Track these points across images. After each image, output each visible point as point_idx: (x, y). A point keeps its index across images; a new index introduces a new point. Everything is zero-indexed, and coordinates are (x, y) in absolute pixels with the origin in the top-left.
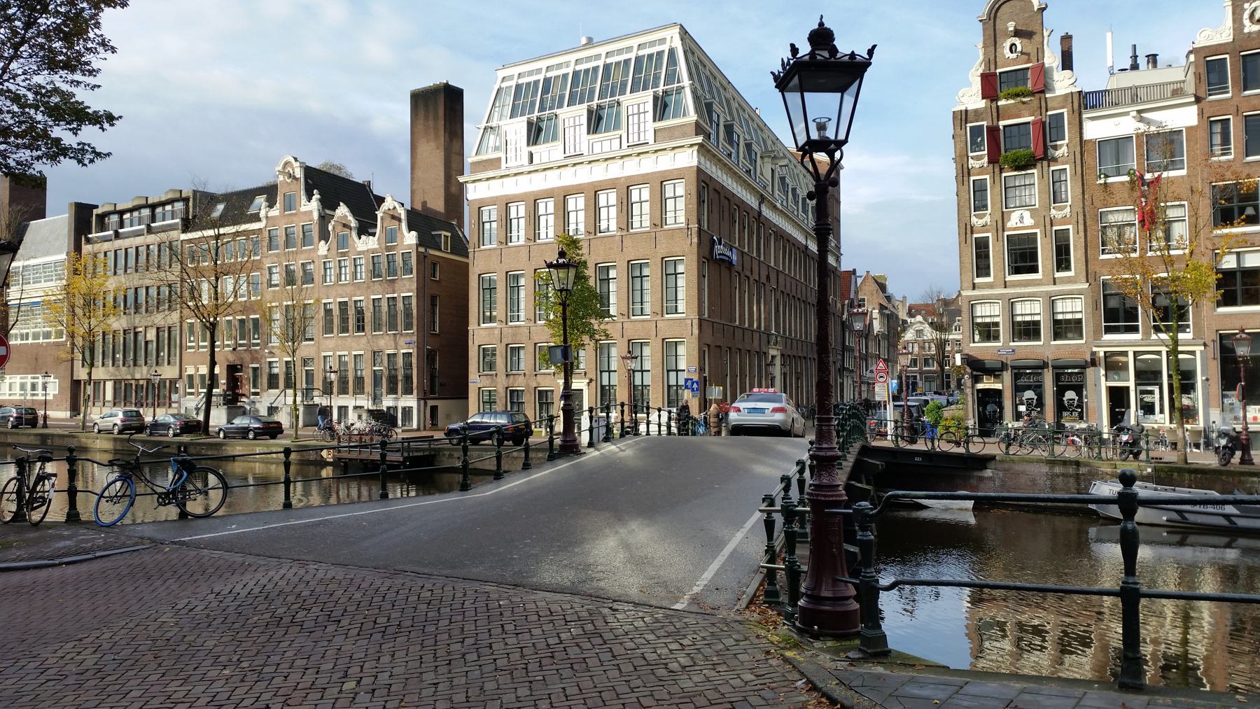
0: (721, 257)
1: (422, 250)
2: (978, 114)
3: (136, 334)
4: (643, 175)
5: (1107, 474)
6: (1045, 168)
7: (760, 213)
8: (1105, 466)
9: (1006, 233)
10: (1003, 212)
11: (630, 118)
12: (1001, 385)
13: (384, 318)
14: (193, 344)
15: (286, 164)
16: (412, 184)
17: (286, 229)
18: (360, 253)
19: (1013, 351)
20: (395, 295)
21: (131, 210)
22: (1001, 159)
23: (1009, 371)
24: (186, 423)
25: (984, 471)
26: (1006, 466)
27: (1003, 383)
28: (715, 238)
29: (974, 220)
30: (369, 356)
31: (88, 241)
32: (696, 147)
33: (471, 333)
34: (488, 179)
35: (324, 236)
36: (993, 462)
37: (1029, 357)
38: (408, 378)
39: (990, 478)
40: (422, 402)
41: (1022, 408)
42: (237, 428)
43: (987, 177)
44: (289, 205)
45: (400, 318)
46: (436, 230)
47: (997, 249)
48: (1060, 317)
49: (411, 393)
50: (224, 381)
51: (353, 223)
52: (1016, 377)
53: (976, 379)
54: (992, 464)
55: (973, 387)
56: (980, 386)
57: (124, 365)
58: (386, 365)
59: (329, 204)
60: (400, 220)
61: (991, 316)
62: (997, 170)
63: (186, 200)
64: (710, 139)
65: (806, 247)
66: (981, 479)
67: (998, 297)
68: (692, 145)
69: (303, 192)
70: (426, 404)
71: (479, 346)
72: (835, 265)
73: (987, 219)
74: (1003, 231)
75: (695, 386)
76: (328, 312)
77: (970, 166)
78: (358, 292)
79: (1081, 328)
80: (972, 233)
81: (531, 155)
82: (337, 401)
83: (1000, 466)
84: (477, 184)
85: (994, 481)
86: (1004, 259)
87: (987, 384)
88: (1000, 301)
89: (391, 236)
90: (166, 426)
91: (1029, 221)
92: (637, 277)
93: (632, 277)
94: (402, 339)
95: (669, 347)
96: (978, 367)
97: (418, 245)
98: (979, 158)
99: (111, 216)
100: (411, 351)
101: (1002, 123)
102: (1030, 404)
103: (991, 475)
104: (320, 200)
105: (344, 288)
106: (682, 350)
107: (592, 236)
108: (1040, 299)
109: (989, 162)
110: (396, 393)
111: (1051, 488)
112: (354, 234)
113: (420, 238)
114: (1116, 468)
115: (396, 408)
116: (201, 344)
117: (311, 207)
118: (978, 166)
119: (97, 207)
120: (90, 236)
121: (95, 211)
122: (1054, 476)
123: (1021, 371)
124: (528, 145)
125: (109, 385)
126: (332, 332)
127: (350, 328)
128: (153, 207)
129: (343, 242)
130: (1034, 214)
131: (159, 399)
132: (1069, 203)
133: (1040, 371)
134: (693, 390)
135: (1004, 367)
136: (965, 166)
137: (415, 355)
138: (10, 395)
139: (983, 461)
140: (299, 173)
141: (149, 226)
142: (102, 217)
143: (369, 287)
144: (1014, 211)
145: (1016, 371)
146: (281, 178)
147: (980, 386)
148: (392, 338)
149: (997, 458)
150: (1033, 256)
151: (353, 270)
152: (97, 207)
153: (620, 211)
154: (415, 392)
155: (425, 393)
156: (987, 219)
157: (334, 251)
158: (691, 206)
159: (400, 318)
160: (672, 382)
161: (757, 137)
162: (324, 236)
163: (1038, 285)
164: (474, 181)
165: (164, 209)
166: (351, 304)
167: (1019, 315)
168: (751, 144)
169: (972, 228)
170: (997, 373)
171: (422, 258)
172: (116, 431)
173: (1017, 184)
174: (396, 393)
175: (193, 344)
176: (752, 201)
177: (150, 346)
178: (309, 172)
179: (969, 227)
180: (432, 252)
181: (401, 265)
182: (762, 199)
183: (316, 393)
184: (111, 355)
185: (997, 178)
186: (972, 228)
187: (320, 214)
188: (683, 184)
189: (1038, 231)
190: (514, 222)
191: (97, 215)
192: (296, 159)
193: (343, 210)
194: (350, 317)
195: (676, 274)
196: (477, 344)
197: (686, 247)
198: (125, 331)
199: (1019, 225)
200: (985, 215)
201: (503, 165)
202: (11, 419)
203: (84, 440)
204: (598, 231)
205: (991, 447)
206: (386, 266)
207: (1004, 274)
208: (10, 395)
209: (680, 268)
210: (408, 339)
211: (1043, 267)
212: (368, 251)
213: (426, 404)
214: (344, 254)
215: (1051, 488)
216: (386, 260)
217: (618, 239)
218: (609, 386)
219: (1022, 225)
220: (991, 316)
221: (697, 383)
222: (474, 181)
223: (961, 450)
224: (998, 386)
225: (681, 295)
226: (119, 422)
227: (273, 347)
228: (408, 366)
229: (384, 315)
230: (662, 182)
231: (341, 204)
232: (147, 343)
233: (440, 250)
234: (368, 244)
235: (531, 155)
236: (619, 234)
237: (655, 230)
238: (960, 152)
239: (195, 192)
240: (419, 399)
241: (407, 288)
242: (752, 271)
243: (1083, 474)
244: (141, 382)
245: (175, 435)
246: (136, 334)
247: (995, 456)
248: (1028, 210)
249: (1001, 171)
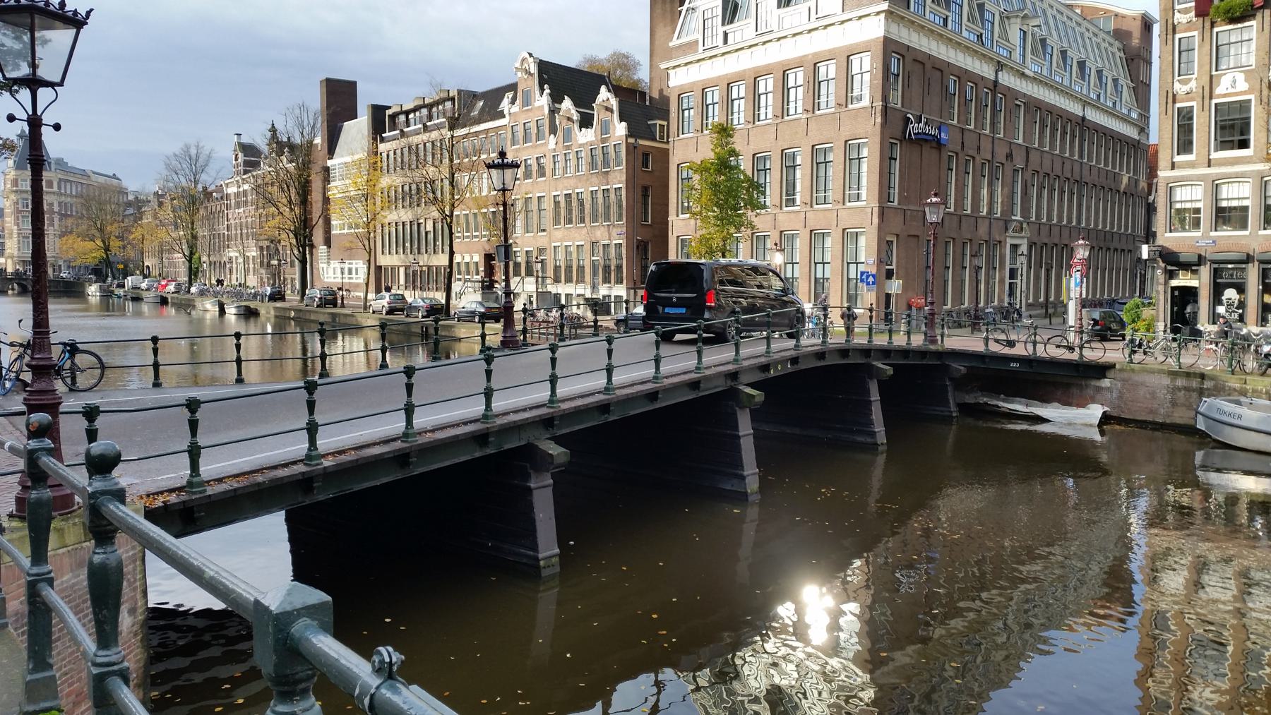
1: (631, 140)
3: (419, 225)
4: (830, 51)
5: (1235, 390)
7: (996, 83)
8: (1233, 381)
9: (1214, 101)
10: (1211, 77)
11: (706, 22)
12: (1197, 282)
13: (600, 210)
14: (460, 235)
15: (524, 60)
16: (651, 72)
17: (524, 124)
18: (581, 145)
19: (1214, 242)
20: (609, 187)
21: (414, 110)
22: (1212, 11)
23: (1208, 266)
24: (432, 307)
25: (1102, 380)
26: (1126, 375)
27: (1200, 280)
29: (1177, 86)
30: (588, 247)
31: (383, 140)
32: (883, 15)
33: (670, 224)
34: (686, 64)
35: (553, 130)
36: (1113, 370)
37: (1232, 249)
38: (619, 267)
39: (1108, 389)
40: (632, 291)
41: (1221, 310)
42: (467, 312)
43: (1195, 33)
44: (527, 102)
45: (613, 209)
46: (652, 120)
47: (1202, 120)
48: (1224, 204)
49: (622, 283)
50: (483, 269)
51: (576, 117)
52: (1216, 273)
53: (1171, 275)
54: (1111, 374)
55: (1166, 283)
57: (411, 253)
58: (602, 255)
59: (556, 98)
60: (612, 111)
61: (1192, 201)
62: (1208, 25)
63: (453, 99)
64: (908, 8)
66: (1099, 389)
67: (1200, 178)
68: (878, 13)
69: (537, 87)
70: (635, 293)
71: (678, 237)
73: (1193, 84)
74: (1211, 98)
75: (871, 279)
76: (557, 203)
77: (1176, 22)
78: (580, 185)
79: (1246, 217)
80: (1174, 102)
81: (726, 35)
82: (563, 289)
83: (1119, 375)
84: (677, 69)
85: (1112, 392)
86: (1209, 133)
87: (1184, 280)
88: (1202, 183)
89: (605, 128)
90: (417, 309)
91: (1242, 85)
92: (762, 170)
93: (817, 163)
94: (615, 230)
95: (847, 237)
96: (1173, 261)
97: (627, 137)
98: (1186, 11)
99: (400, 116)
100: (621, 241)
102: (1230, 305)
103: (1109, 385)
104: (550, 95)
105: (569, 180)
106: (862, 241)
107: (779, 120)
108: (1250, 180)
109: (1197, 16)
110: (610, 282)
111: (1171, 402)
112: (576, 127)
113: (629, 128)
114: (1245, 383)
115: (609, 296)
116: (466, 234)
117: (542, 101)
118: (1184, 21)
119: (389, 108)
120: (384, 135)
121: (389, 112)
122: (1176, 389)
123: (1222, 266)
124: (723, 24)
125: (402, 270)
126: (560, 224)
127: (574, 219)
128: (430, 107)
129: (567, 136)
131: (437, 284)
133: (1244, 266)
134: (868, 284)
135: (1201, 260)
136: (1170, 22)
137: (624, 245)
138: (334, 278)
139: (1101, 370)
140: (533, 69)
141: (425, 126)
142: (393, 117)
143: (588, 180)
144: (1225, 74)
145: (1216, 266)
146: (519, 74)
147: (1174, 283)
148: (606, 229)
149: (1117, 366)
150: (1245, 127)
151: (576, 163)
152: (389, 108)
153: (806, 92)
154: (625, 281)
155: (635, 283)
156: (1193, 84)
157: (560, 145)
158: (876, 82)
159: (613, 209)
160: (852, 275)
162: (553, 130)
163: (1249, 163)
164: (674, 67)
165: (438, 108)
166: (574, 196)
167: (1178, 202)
169: (1174, 96)
170: (1194, 268)
171: (631, 149)
172: (384, 312)
173: (1232, 40)
174: (610, 282)
175: (460, 235)
176: (987, 71)
177: (429, 236)
178: (544, 67)
179: (1170, 95)
180: (642, 142)
181: (614, 157)
182: (1000, 66)
183: (548, 281)
184: (402, 244)
185: (1207, 34)
186: (1174, 96)
187: (550, 108)
189: (1251, 97)
190: (857, 79)
191: (389, 116)
192: (531, 55)
193: (567, 104)
194: (574, 208)
195: (859, 159)
196: (675, 235)
197: (869, 128)
198: (411, 222)
200: (1190, 80)
201: (701, 48)
202: (317, 299)
203: (359, 319)
204: (756, 119)
205: (1113, 353)
206: (602, 159)
207: (1209, 151)
208: (334, 278)
209: (865, 152)
210: (619, 230)
211: (1255, 141)
212: (587, 143)
213: (635, 293)
214: (568, 148)
215: (1171, 402)
216: (601, 152)
217: (804, 122)
218: (793, 278)
220: (1192, 201)
221: (874, 276)
222: (674, 67)
223: (1075, 356)
224: (1194, 283)
225: (864, 181)
226: (386, 305)
227: (517, 238)
228: (619, 257)
229: (600, 206)
230: (703, 89)
231: (566, 97)
232: (426, 233)
233: (654, 139)
234: (586, 137)
235: (726, 35)
236: (805, 116)
237: (839, 111)
238: (1165, 5)
239: (459, 92)
240: (628, 289)
241: (618, 180)
242: (979, 148)
243: (1208, 389)
244: (424, 268)
245: (423, 317)
246: (419, 225)
247: (1115, 365)
249: (1213, 25)
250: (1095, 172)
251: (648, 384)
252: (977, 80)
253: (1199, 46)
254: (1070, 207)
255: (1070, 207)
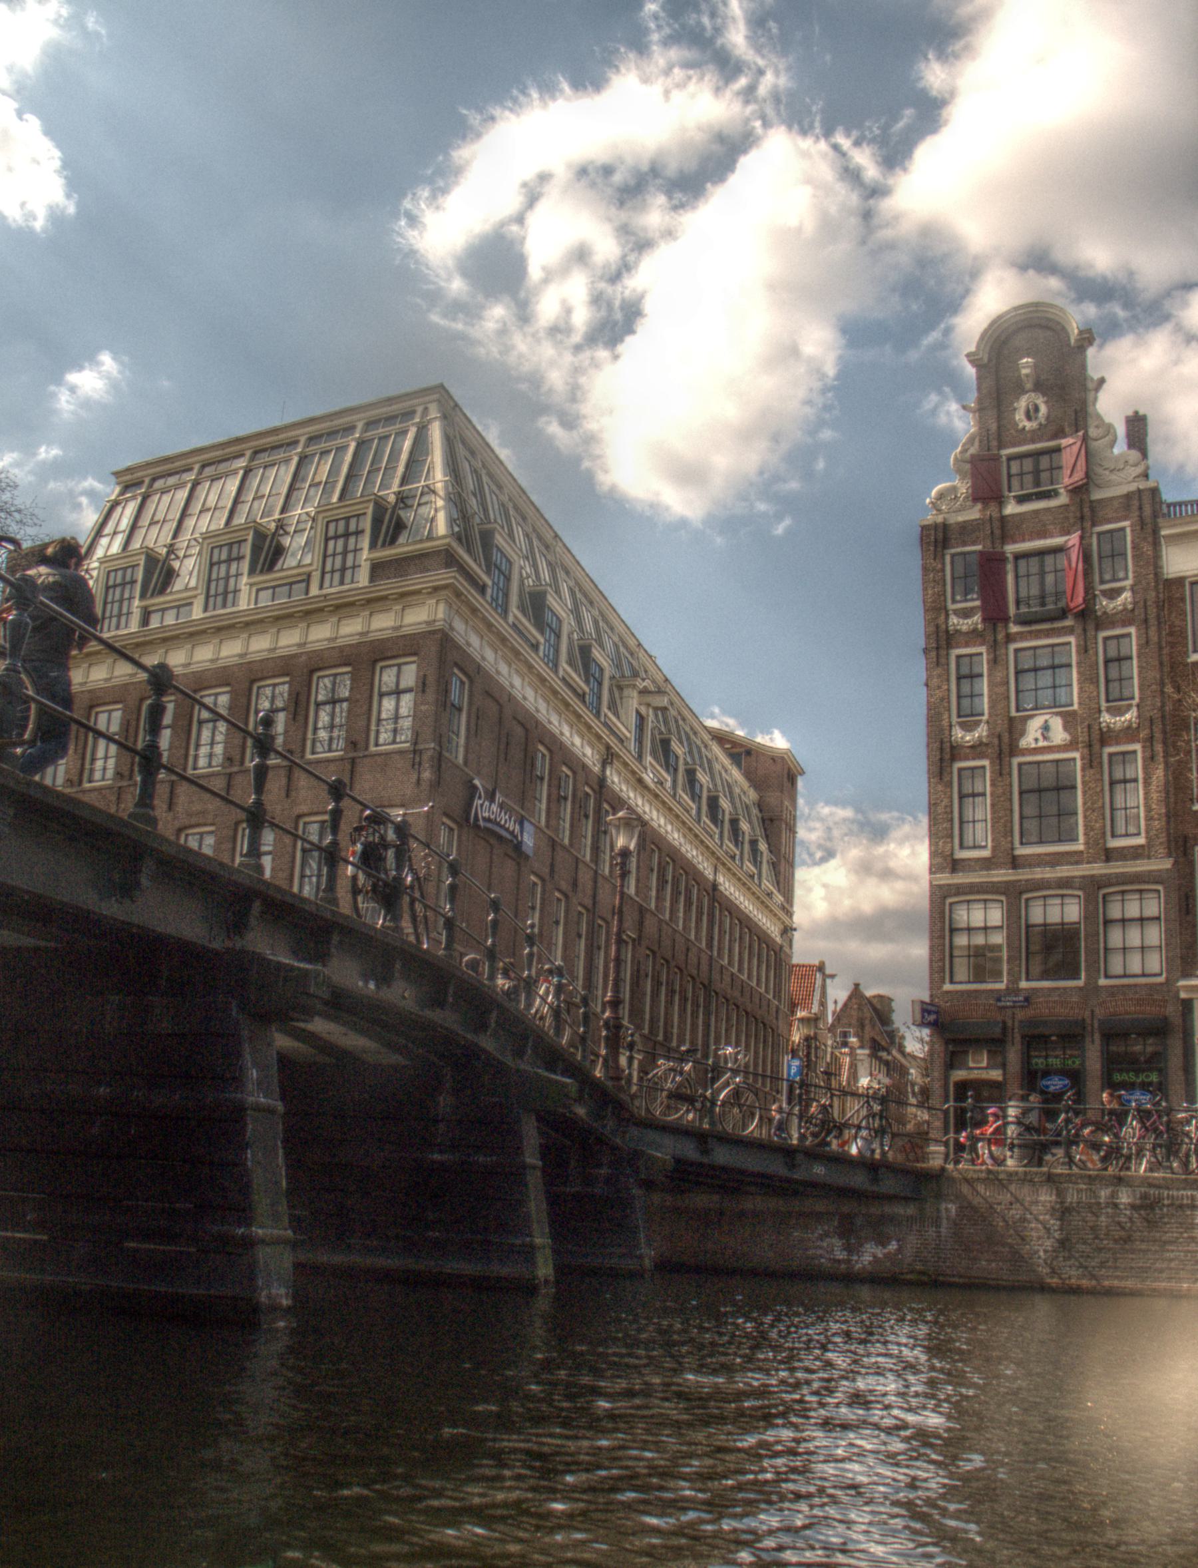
0: (489, 825)
2: (967, 531)
6: (1091, 633)
12: (1000, 1072)
28: (477, 782)
56: (959, 1075)
65: (715, 886)
72: (778, 940)
91: (1059, 735)
98: (966, 614)
101: (1011, 548)
130: (1069, 720)
132: (1136, 700)
161: (701, 757)
168: (590, 646)
176: (589, 754)
182: (609, 757)
188: (414, 667)
199: (1041, 744)
200: (978, 723)
219: (1046, 744)
248: (1057, 714)
250: (727, 979)
251: (197, 493)
252: (577, 766)
253: (989, 670)
254: (694, 1026)
255: (694, 1026)
